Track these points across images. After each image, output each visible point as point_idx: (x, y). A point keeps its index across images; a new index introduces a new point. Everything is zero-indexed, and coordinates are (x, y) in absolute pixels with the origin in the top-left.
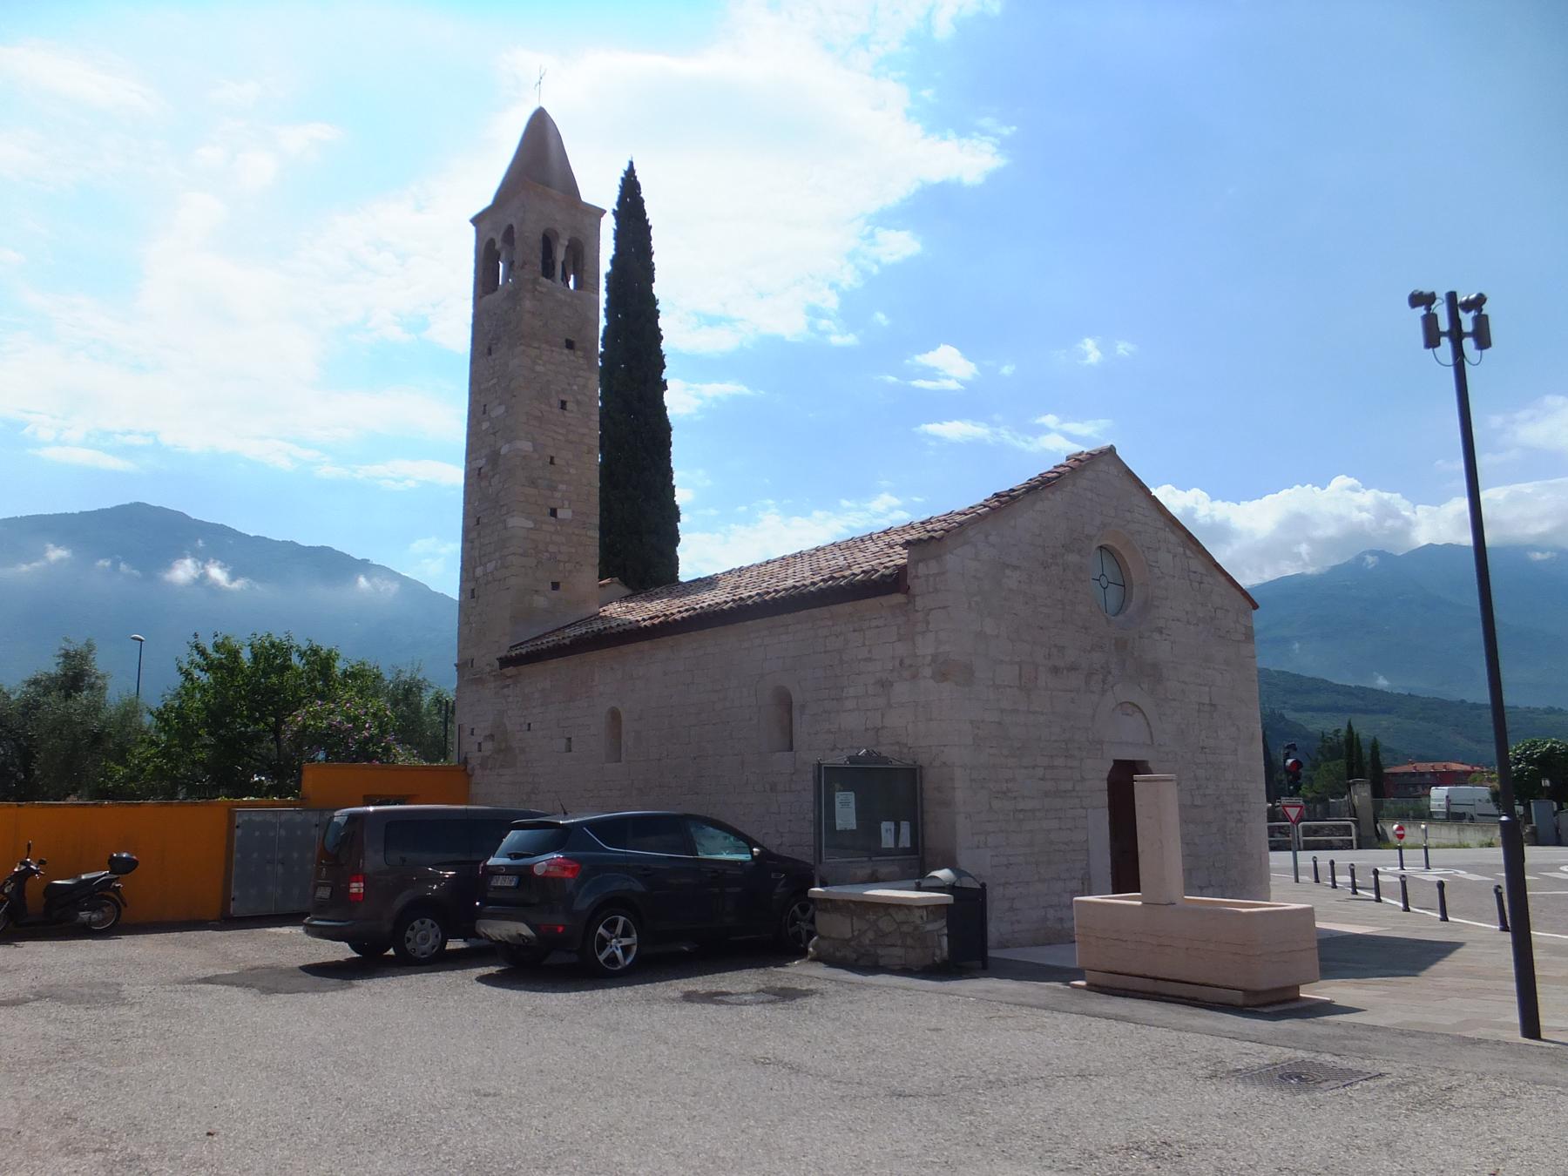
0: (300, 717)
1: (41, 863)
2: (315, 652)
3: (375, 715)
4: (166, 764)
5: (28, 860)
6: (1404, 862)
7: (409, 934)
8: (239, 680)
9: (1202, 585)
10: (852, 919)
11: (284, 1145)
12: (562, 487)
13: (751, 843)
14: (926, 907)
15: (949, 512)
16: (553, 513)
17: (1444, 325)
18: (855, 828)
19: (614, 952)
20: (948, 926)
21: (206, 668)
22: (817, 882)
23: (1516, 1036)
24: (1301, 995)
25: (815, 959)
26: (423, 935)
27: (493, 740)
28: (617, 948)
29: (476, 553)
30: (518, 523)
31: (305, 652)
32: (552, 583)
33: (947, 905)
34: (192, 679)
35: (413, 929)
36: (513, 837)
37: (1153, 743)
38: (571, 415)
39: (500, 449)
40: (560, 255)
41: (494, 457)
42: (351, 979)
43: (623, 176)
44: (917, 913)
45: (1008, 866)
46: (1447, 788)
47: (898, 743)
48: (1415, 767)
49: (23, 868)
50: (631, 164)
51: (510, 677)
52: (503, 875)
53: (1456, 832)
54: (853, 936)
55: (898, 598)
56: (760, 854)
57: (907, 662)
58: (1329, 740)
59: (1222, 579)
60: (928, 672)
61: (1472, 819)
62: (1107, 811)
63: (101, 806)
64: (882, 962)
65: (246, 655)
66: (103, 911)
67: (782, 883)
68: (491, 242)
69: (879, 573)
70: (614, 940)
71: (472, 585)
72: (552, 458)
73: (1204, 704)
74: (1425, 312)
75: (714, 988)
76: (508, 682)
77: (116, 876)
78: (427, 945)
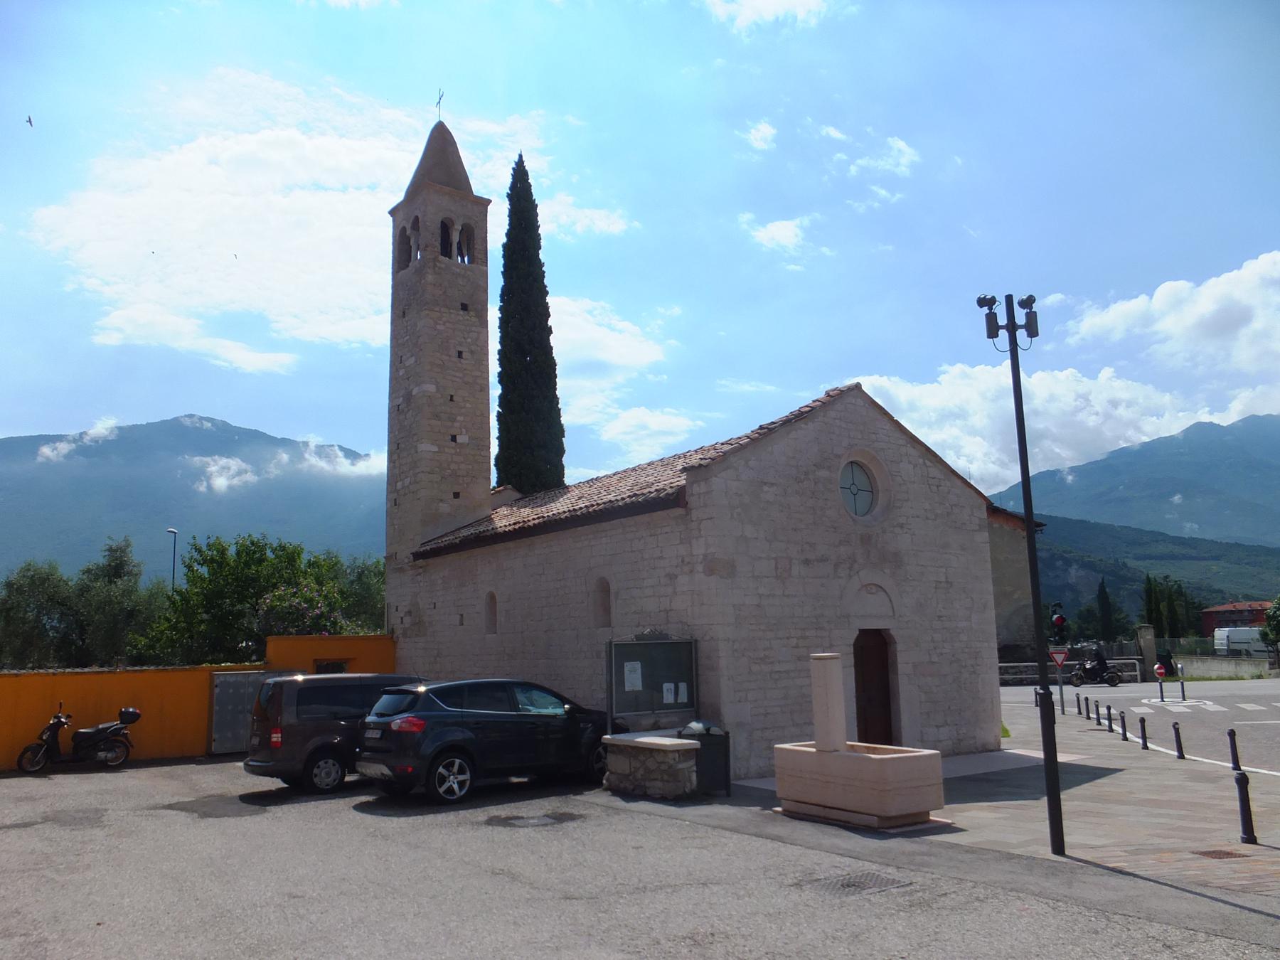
0: (268, 599)
1: (68, 717)
2: (283, 548)
3: (326, 596)
4: (175, 635)
5: (60, 715)
6: (1164, 694)
7: (316, 771)
8: (226, 571)
9: (940, 488)
10: (630, 760)
11: (142, 932)
12: (459, 418)
13: (563, 700)
14: (678, 751)
15: (700, 447)
16: (454, 438)
17: (1002, 320)
18: (641, 689)
19: (451, 785)
20: (697, 764)
21: (202, 562)
22: (609, 730)
23: (1046, 851)
24: (931, 818)
25: (606, 790)
26: (325, 772)
27: (411, 616)
28: (454, 783)
29: (397, 471)
30: (426, 447)
31: (276, 549)
32: (454, 493)
33: (696, 750)
34: (193, 571)
35: (326, 763)
36: (385, 698)
37: (894, 615)
38: (466, 362)
39: (411, 391)
40: (455, 237)
41: (408, 397)
42: (265, 806)
43: (514, 166)
44: (671, 756)
45: (766, 714)
46: (1227, 629)
47: (681, 622)
48: (1235, 606)
49: (56, 720)
50: (521, 156)
51: (421, 567)
52: (372, 729)
53: (1234, 666)
54: (631, 771)
55: (679, 511)
56: (570, 709)
57: (687, 560)
58: (1159, 585)
59: (959, 482)
60: (700, 568)
61: (1248, 654)
62: (853, 669)
63: (114, 673)
64: (649, 792)
65: (232, 551)
66: (115, 751)
67: (589, 730)
68: (404, 229)
69: (666, 492)
70: (452, 777)
71: (395, 496)
72: (452, 396)
73: (940, 582)
74: (988, 311)
75: (515, 814)
76: (421, 570)
77: (124, 726)
78: (330, 779)
